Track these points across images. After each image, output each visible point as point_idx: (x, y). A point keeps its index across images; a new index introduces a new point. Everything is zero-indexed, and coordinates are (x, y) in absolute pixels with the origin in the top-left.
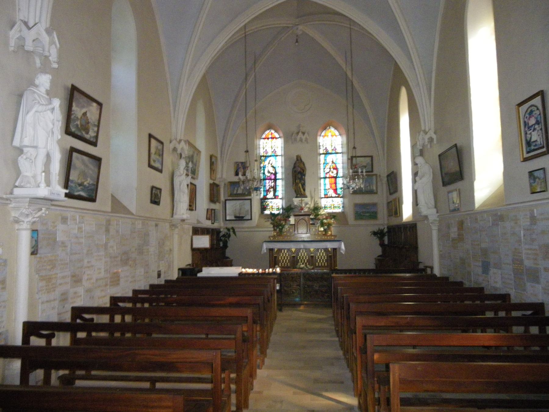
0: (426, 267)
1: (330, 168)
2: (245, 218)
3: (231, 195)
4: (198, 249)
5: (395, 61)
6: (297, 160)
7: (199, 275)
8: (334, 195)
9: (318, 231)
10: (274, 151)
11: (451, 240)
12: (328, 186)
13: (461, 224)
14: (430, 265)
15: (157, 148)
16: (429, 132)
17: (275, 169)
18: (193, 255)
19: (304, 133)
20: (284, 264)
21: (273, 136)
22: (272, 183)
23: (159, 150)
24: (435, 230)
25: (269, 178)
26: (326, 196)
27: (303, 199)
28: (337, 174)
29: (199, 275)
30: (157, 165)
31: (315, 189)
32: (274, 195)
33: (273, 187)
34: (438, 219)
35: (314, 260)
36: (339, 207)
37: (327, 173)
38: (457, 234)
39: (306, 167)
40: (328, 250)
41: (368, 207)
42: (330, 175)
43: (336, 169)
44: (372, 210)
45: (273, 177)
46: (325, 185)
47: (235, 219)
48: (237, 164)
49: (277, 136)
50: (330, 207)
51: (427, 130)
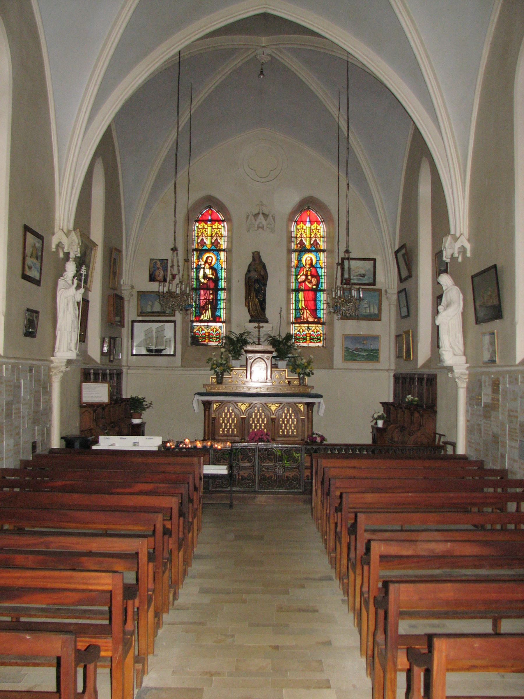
0: (446, 443)
1: (306, 275)
2: (164, 353)
3: (141, 313)
4: (91, 406)
5: (416, 129)
6: (254, 259)
7: (94, 447)
8: (311, 319)
9: (284, 378)
10: (216, 243)
11: (483, 405)
12: (301, 305)
13: (495, 385)
14: (452, 441)
15: (34, 246)
16: (460, 239)
17: (216, 273)
18: (82, 414)
19: (265, 216)
20: (228, 431)
21: (215, 217)
22: (210, 294)
23: (37, 249)
24: (462, 388)
25: (205, 286)
26: (299, 321)
27: (261, 325)
28: (317, 285)
29: (94, 447)
30: (34, 274)
31: (281, 308)
32: (213, 315)
33: (211, 303)
34: (467, 372)
35: (276, 424)
36: (318, 339)
37: (300, 283)
38: (490, 397)
39: (268, 272)
40: (300, 409)
41: (365, 342)
42: (305, 285)
43: (317, 276)
44: (372, 347)
45: (212, 285)
46: (297, 301)
47: (149, 353)
48: (153, 262)
49: (221, 217)
50: (304, 339)
51: (458, 235)
